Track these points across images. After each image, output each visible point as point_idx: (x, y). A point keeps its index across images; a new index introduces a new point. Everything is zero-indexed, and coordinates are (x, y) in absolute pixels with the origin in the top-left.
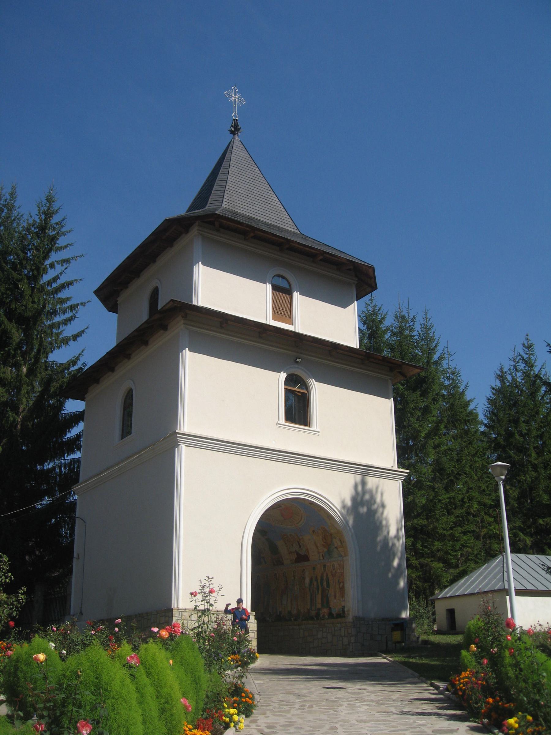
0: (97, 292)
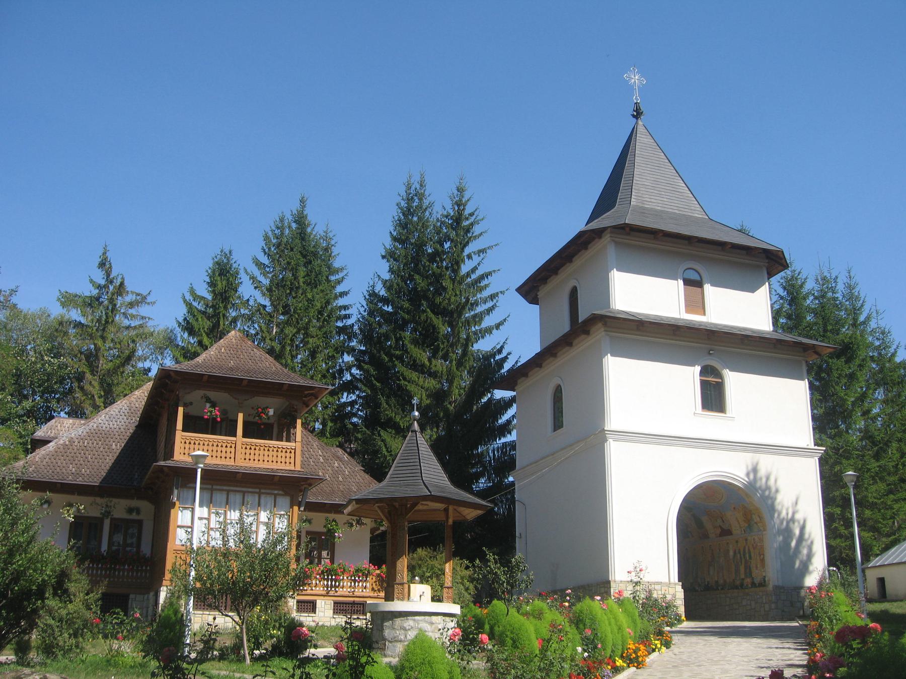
0: (519, 290)
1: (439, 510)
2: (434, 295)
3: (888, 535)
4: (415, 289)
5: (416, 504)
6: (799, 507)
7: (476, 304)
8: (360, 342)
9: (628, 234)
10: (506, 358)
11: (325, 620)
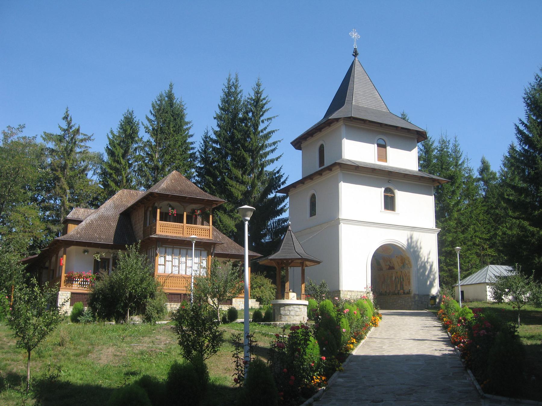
0: (291, 143)
3: (466, 271)
6: (430, 256)
8: (200, 162)
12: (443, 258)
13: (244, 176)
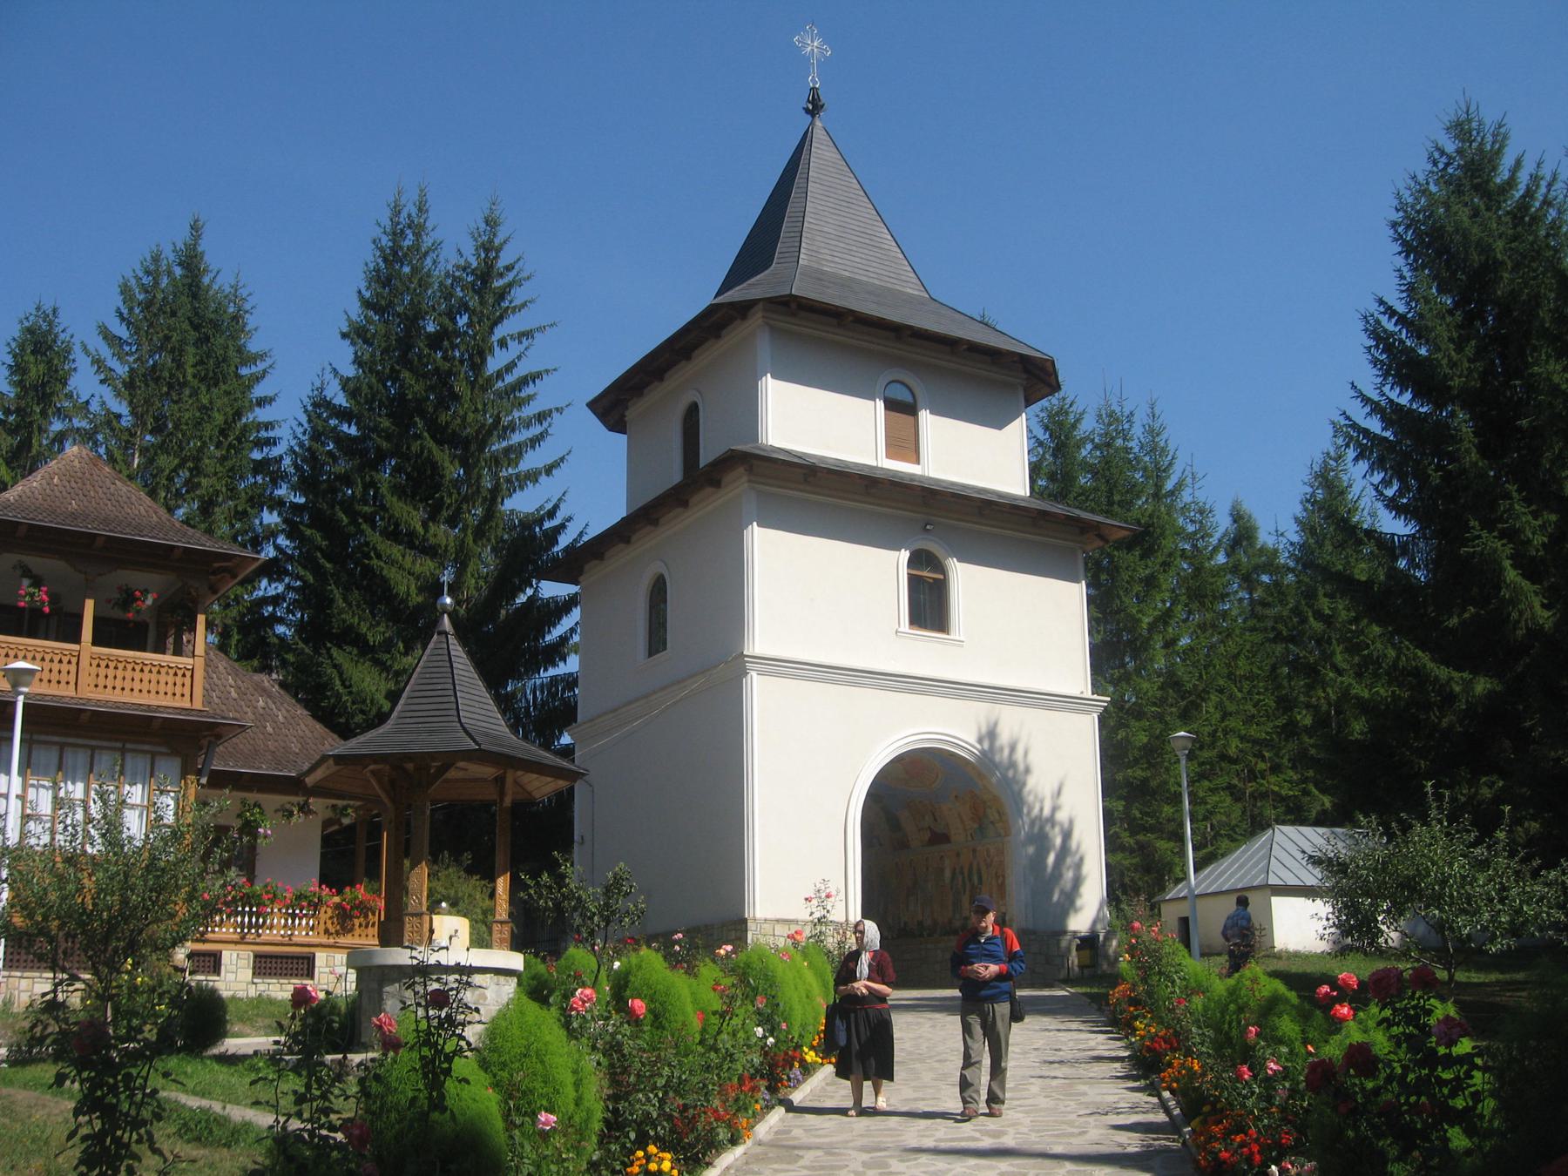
0: (593, 405)
1: (485, 780)
2: (436, 409)
4: (401, 396)
5: (446, 767)
6: (1064, 799)
7: (512, 427)
8: (293, 488)
9: (794, 315)
10: (562, 527)
11: (234, 986)
12: (1119, 805)
13: (432, 527)
